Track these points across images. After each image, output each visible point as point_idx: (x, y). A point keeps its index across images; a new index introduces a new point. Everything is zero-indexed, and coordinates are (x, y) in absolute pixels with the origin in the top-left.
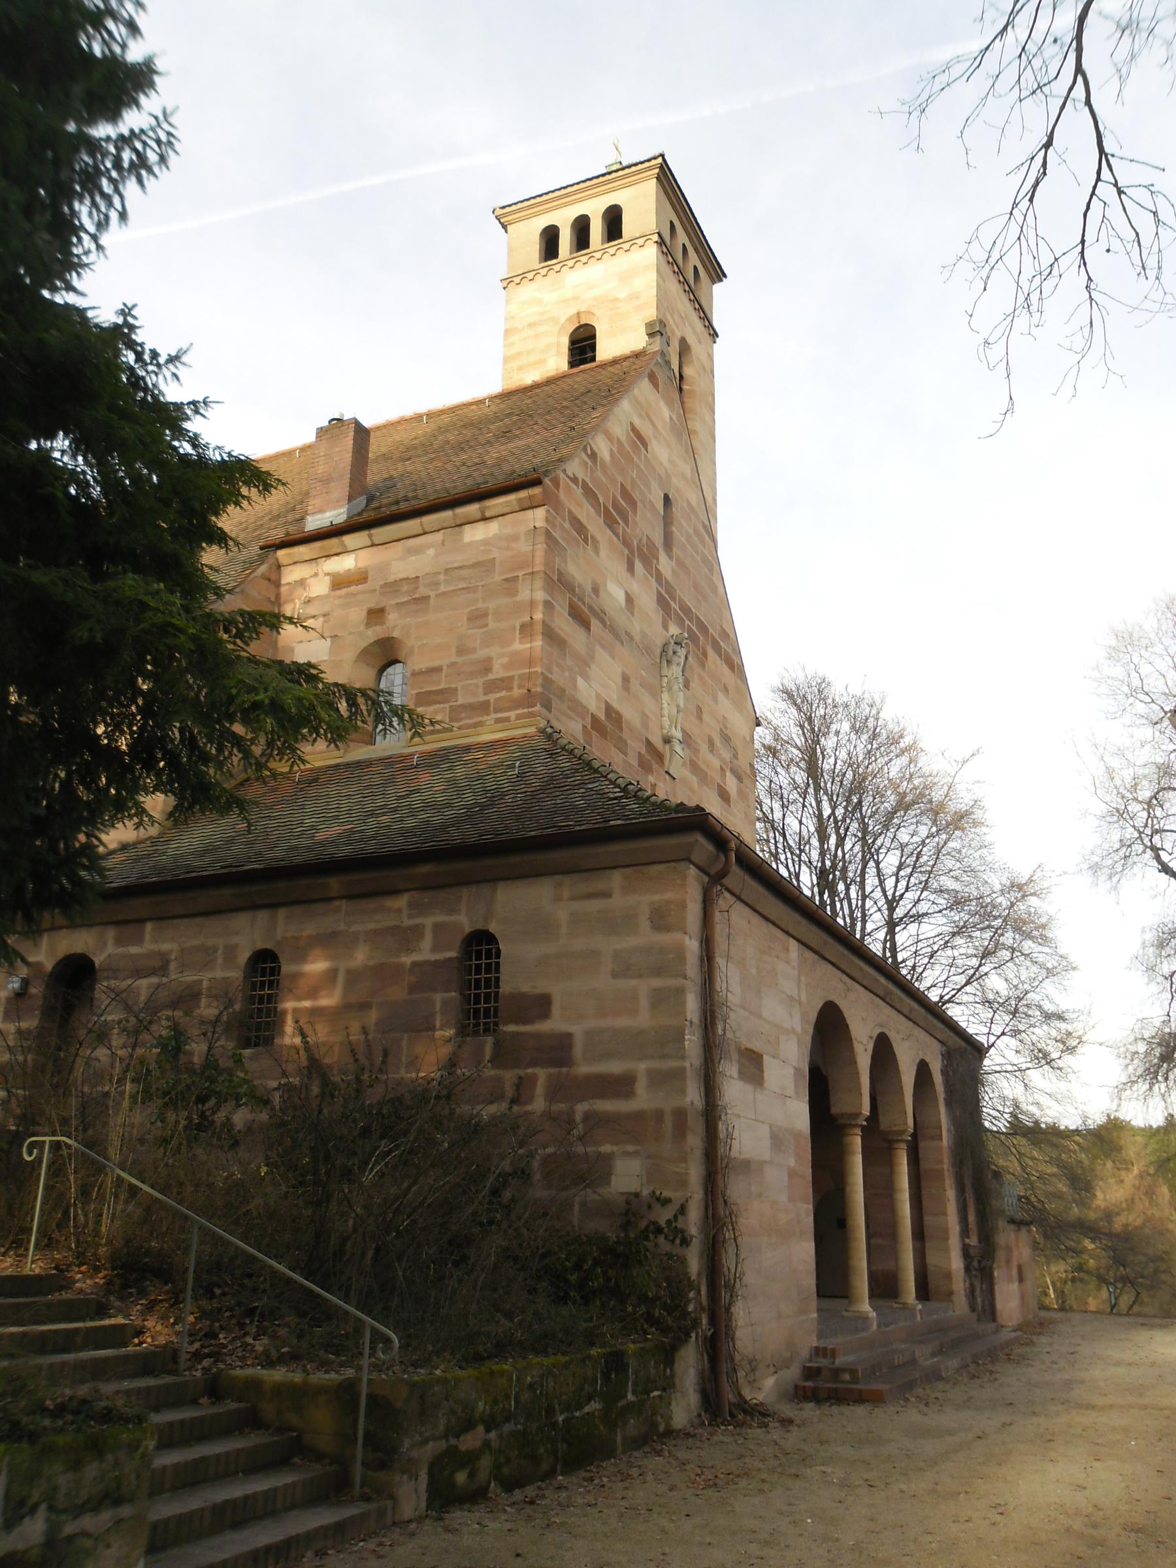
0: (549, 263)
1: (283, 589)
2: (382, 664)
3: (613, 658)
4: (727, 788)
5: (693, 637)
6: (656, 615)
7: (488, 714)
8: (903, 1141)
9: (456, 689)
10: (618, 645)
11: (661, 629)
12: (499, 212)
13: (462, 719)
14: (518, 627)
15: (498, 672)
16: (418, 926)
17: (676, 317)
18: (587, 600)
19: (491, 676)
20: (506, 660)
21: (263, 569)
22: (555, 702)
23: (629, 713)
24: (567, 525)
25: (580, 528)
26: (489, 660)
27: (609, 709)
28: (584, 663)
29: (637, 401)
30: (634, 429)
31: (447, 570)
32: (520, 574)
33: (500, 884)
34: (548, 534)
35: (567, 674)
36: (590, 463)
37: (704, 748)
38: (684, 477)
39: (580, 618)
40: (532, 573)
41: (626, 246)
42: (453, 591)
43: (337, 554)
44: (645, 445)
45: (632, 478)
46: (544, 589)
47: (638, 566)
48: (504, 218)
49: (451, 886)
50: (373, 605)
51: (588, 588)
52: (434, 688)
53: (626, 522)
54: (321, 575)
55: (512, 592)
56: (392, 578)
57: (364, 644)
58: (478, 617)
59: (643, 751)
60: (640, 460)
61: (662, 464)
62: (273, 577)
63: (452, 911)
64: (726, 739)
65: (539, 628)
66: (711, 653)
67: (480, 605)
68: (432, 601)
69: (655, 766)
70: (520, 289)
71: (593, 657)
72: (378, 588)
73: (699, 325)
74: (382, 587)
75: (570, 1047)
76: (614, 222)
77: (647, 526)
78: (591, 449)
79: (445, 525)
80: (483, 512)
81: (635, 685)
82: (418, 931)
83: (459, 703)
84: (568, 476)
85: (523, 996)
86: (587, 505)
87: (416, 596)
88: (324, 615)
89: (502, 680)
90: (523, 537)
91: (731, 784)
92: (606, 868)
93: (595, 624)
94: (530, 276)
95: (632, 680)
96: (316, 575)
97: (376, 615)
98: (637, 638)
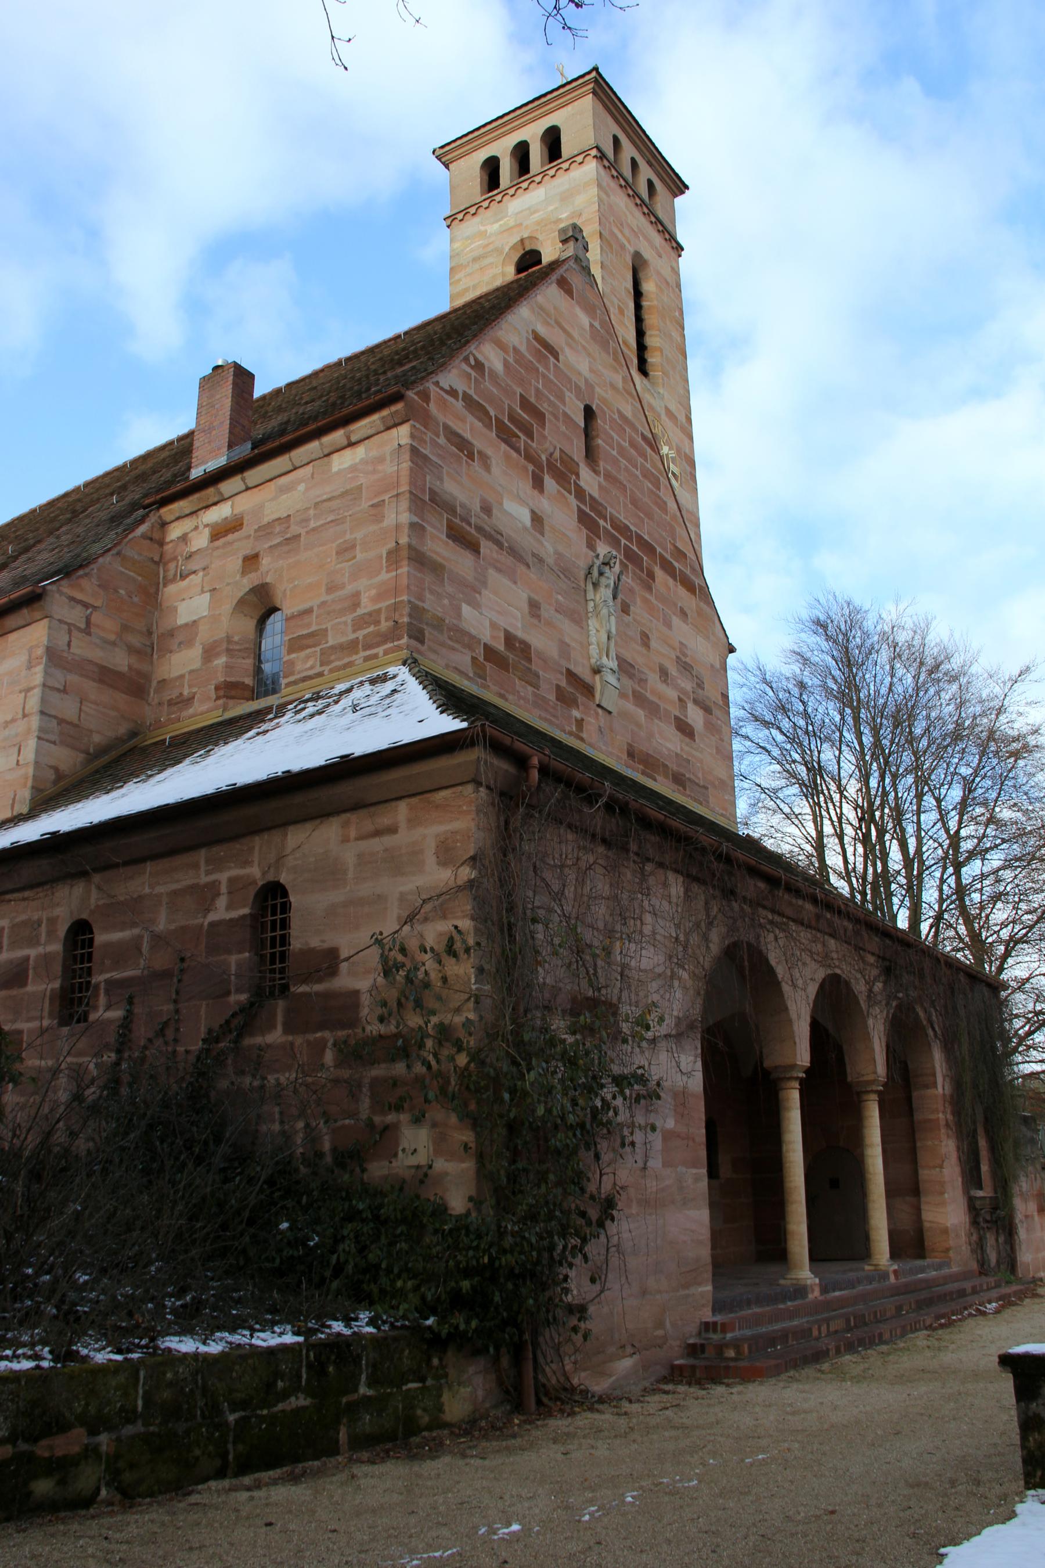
0: (491, 194)
1: (168, 548)
2: (257, 615)
3: (515, 583)
4: (690, 721)
5: (629, 555)
6: (577, 537)
7: (357, 653)
8: (872, 1091)
9: (326, 630)
10: (523, 568)
11: (585, 549)
12: (438, 153)
13: (331, 662)
14: (384, 556)
15: (366, 606)
16: (214, 882)
17: (626, 231)
18: (473, 520)
19: (360, 611)
20: (373, 592)
21: (143, 529)
22: (428, 631)
23: (538, 640)
24: (442, 440)
25: (463, 445)
26: (357, 594)
27: (510, 639)
28: (471, 591)
29: (541, 308)
30: (537, 337)
31: (316, 504)
32: (386, 497)
33: (291, 828)
34: (414, 451)
35: (446, 602)
36: (473, 374)
37: (653, 679)
38: (613, 387)
39: (463, 538)
40: (397, 495)
41: (565, 166)
42: (322, 525)
43: (215, 504)
44: (555, 355)
45: (537, 390)
46: (410, 510)
47: (549, 482)
48: (446, 154)
49: (244, 835)
50: (248, 552)
51: (476, 507)
52: (305, 632)
53: (530, 435)
54: (201, 527)
55: (379, 518)
56: (266, 520)
57: (241, 594)
58: (346, 550)
59: (563, 683)
60: (548, 370)
61: (580, 374)
62: (156, 536)
63: (247, 863)
64: (686, 667)
65: (405, 553)
66: (659, 573)
67: (348, 537)
68: (302, 539)
69: (581, 699)
70: (464, 224)
71: (484, 584)
72: (252, 532)
73: (658, 239)
74: (256, 531)
75: (356, 1006)
76: (553, 140)
77: (560, 438)
78: (476, 359)
79: (313, 457)
80: (348, 438)
81: (547, 611)
82: (213, 889)
83: (330, 643)
84: (442, 389)
85: (312, 951)
86: (470, 418)
87: (288, 536)
88: (204, 569)
89: (370, 614)
90: (388, 458)
91: (695, 716)
92: (386, 801)
93: (486, 547)
94: (472, 210)
95: (544, 606)
96: (196, 528)
97: (251, 561)
98: (550, 561)
